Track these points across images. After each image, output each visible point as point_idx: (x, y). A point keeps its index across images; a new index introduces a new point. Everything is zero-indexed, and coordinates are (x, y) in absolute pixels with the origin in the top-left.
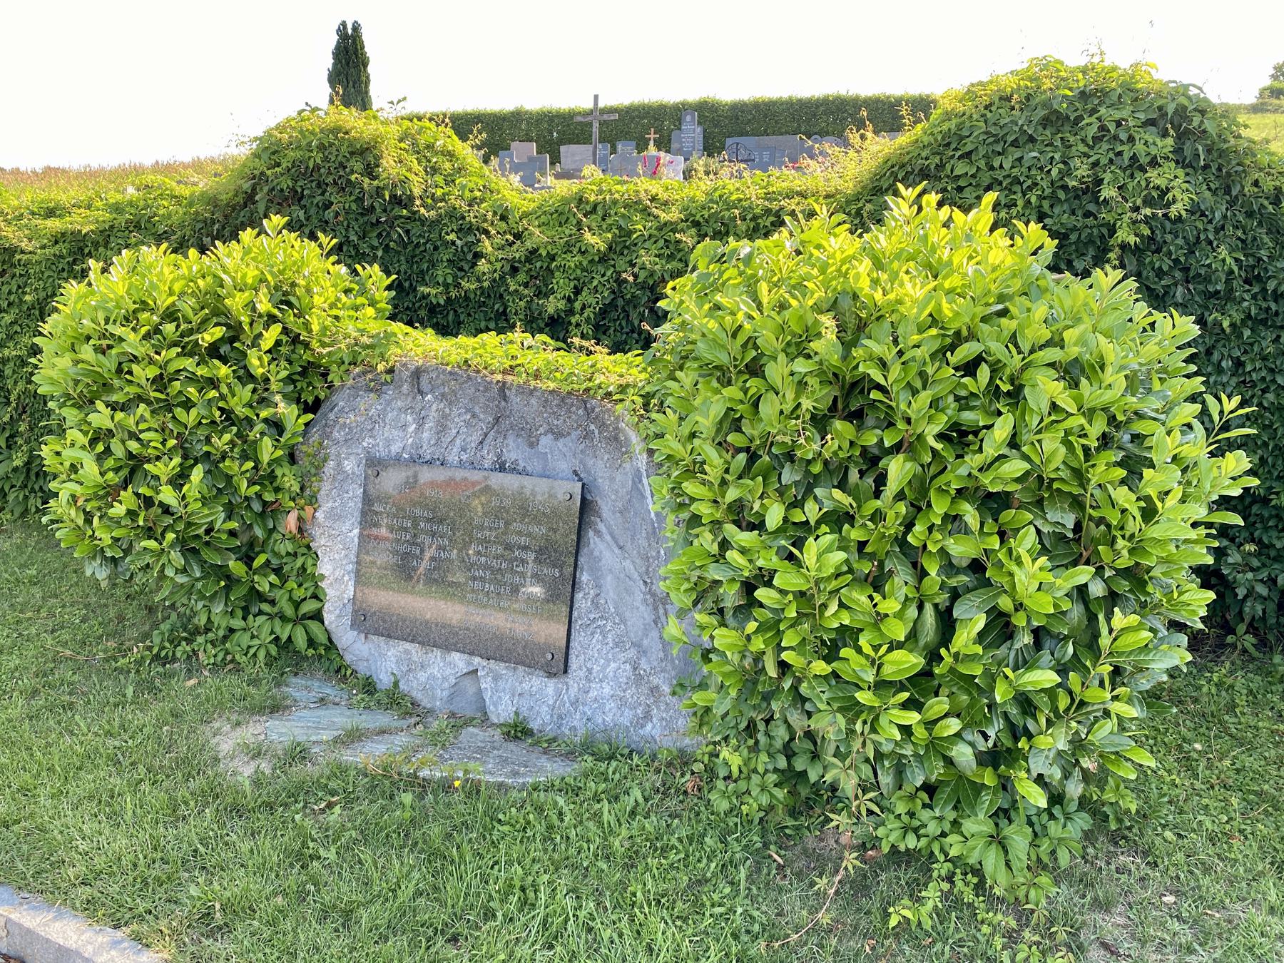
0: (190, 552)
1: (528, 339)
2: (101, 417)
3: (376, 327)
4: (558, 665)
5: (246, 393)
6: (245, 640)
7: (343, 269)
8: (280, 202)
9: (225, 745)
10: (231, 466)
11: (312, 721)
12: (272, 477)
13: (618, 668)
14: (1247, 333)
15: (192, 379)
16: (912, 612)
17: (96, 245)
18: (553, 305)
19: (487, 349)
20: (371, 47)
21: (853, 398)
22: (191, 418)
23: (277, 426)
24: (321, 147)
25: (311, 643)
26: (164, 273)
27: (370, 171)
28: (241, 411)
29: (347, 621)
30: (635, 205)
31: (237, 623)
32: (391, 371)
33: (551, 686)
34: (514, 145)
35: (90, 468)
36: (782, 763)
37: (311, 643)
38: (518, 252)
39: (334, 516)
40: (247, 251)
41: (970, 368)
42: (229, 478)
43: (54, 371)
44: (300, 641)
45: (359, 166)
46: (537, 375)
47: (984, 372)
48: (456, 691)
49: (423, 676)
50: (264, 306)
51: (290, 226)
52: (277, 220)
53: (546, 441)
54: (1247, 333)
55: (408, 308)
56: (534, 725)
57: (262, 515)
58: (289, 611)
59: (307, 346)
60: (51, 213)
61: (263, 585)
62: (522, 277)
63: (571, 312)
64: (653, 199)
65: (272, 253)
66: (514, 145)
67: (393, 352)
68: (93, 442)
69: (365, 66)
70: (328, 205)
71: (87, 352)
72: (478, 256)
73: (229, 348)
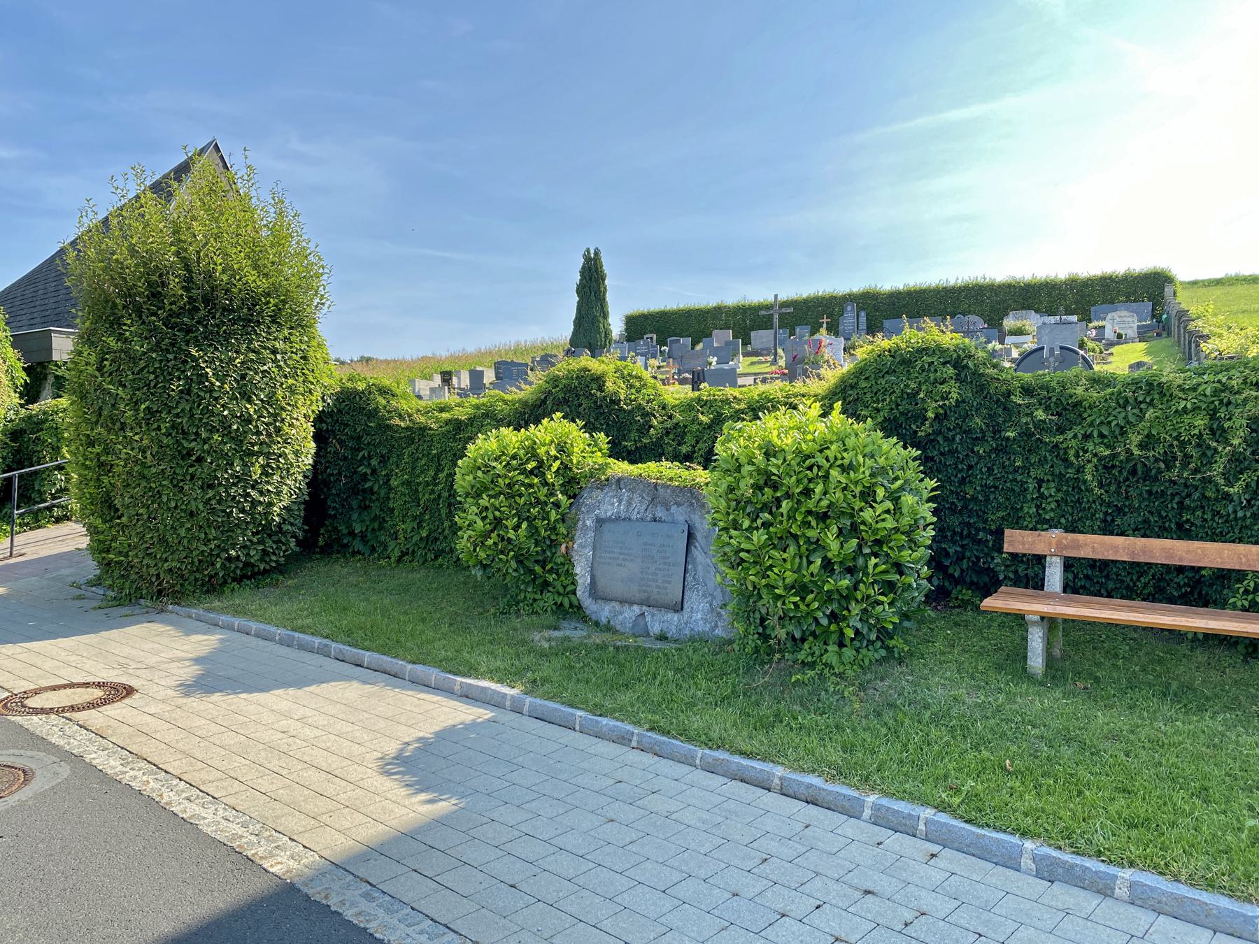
0: (520, 562)
1: (669, 464)
2: (484, 502)
3: (600, 461)
4: (679, 607)
5: (545, 490)
6: (542, 603)
7: (587, 435)
8: (559, 404)
9: (537, 638)
10: (538, 523)
11: (573, 632)
12: (554, 528)
13: (704, 606)
14: (993, 456)
15: (523, 484)
16: (797, 560)
17: (466, 425)
18: (684, 449)
19: (650, 469)
20: (607, 266)
21: (768, 481)
22: (522, 501)
23: (557, 505)
24: (578, 378)
25: (571, 606)
26: (511, 438)
27: (601, 389)
28: (542, 498)
29: (587, 594)
30: (727, 402)
31: (538, 597)
32: (607, 480)
33: (676, 617)
34: (715, 332)
35: (480, 523)
36: (760, 630)
37: (571, 606)
38: (669, 424)
39: (582, 546)
40: (546, 429)
41: (810, 468)
42: (536, 528)
43: (463, 481)
44: (566, 604)
45: (595, 386)
46: (671, 479)
47: (815, 469)
48: (635, 623)
49: (621, 618)
50: (553, 452)
51: (564, 417)
52: (559, 414)
53: (674, 508)
54: (993, 456)
55: (617, 452)
56: (669, 635)
57: (550, 546)
58: (561, 590)
59: (571, 469)
60: (442, 410)
61: (551, 577)
62: (671, 436)
63: (694, 452)
64: (735, 398)
65: (555, 430)
66: (715, 332)
67: (609, 472)
68: (481, 512)
69: (603, 280)
70: (580, 405)
71: (480, 473)
72: (651, 426)
73: (539, 471)
